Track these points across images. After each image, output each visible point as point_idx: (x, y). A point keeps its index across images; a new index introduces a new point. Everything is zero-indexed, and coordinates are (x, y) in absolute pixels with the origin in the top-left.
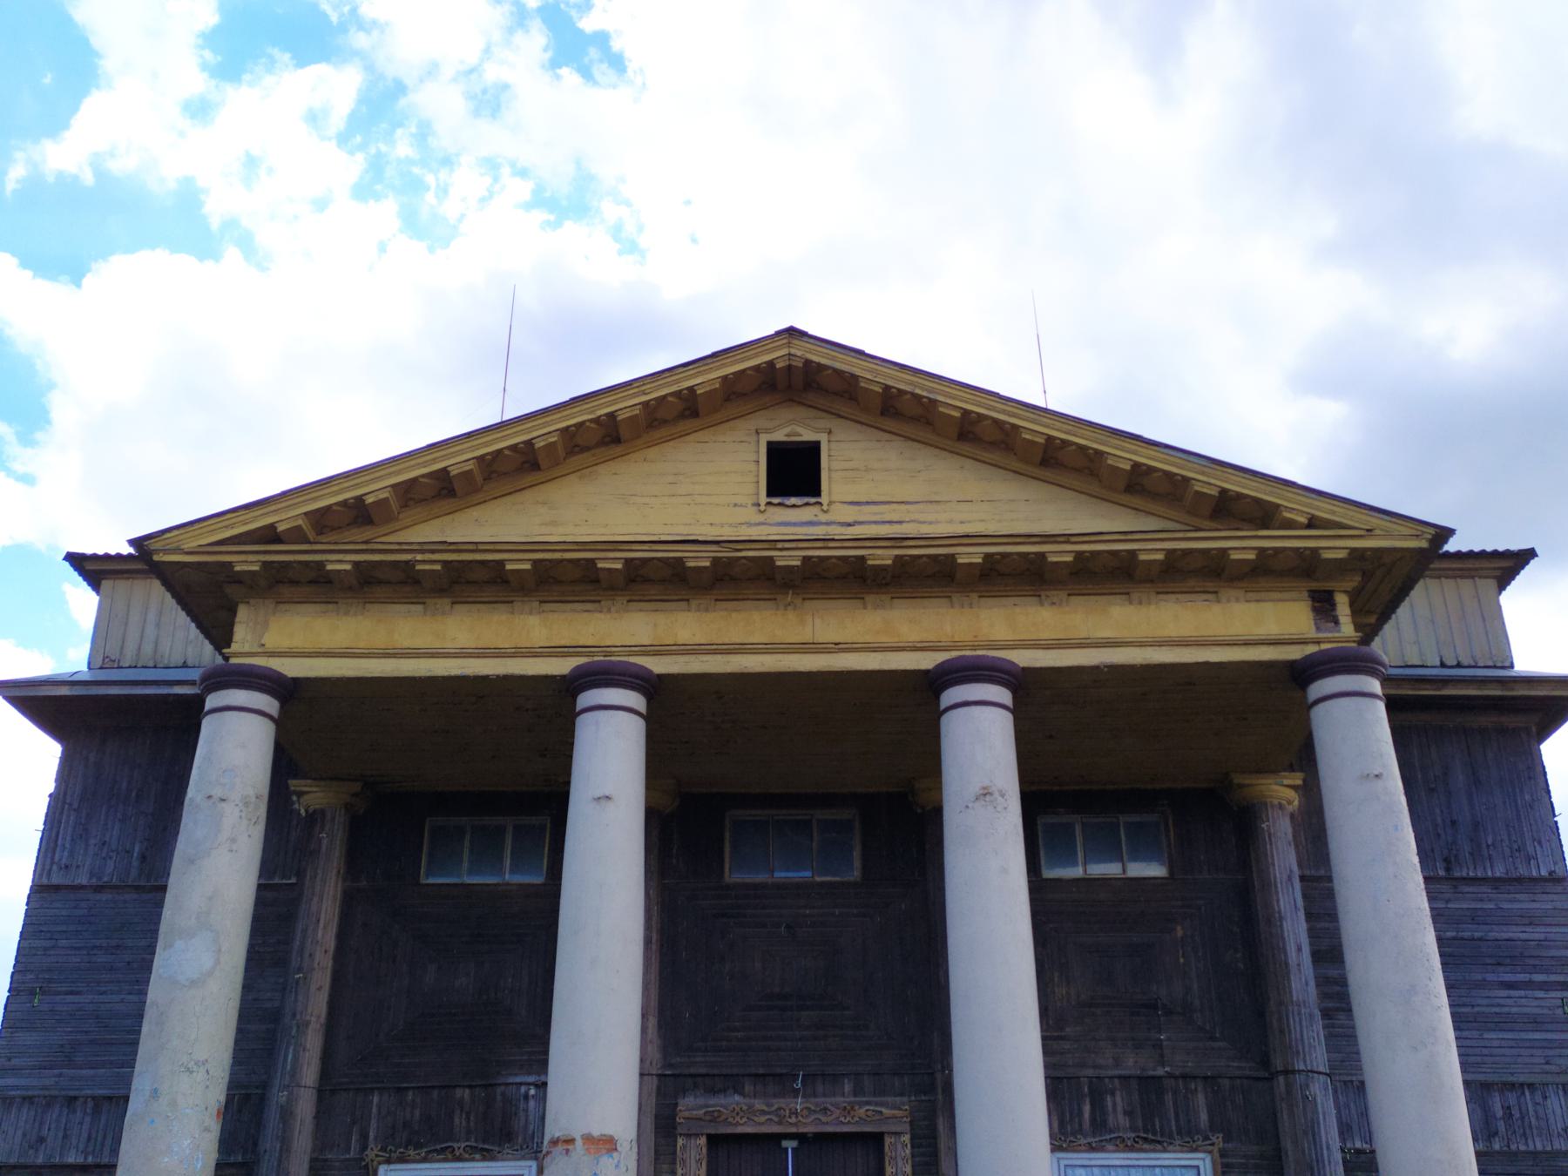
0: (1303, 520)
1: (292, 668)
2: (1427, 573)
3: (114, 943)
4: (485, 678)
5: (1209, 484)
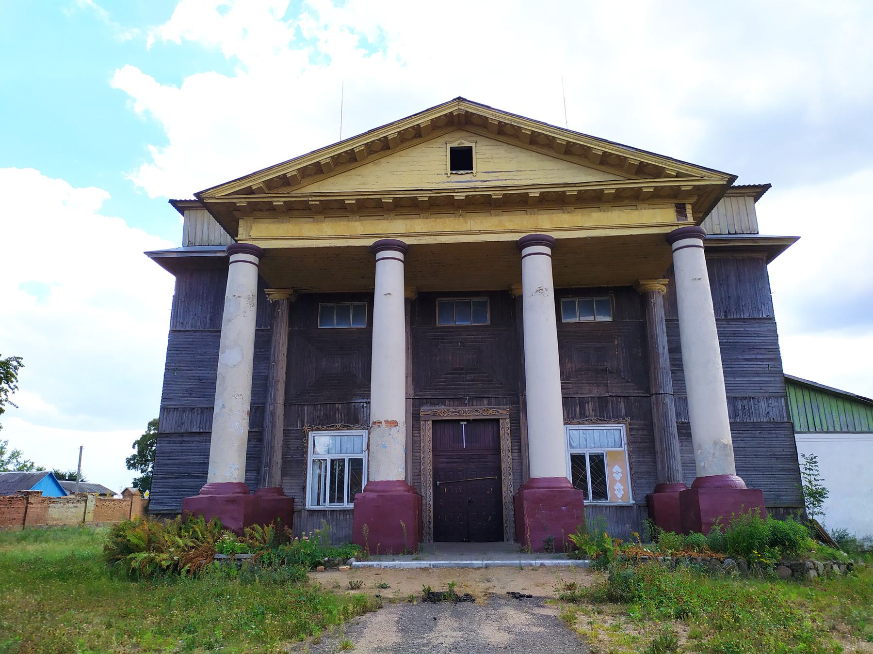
1: (263, 245)
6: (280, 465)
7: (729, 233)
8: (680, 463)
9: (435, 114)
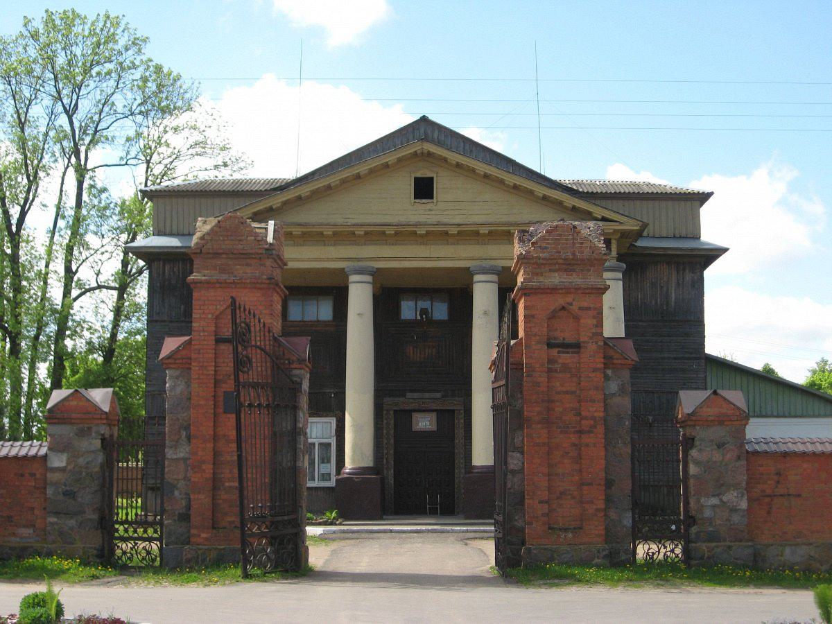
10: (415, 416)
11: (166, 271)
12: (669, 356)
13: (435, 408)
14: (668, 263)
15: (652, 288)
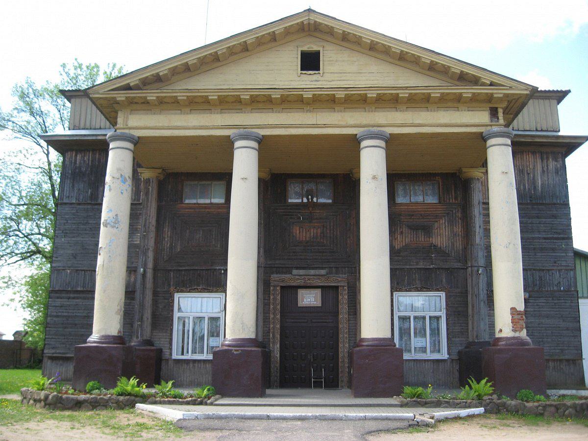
0: (488, 82)
1: (138, 133)
2: (533, 97)
3: (85, 222)
4: (203, 136)
5: (457, 69)
6: (150, 320)
7: (537, 130)
8: (487, 325)
9: (288, 22)
10: (301, 292)
11: (78, 160)
12: (540, 236)
13: (321, 284)
14: (534, 153)
15: (520, 175)
